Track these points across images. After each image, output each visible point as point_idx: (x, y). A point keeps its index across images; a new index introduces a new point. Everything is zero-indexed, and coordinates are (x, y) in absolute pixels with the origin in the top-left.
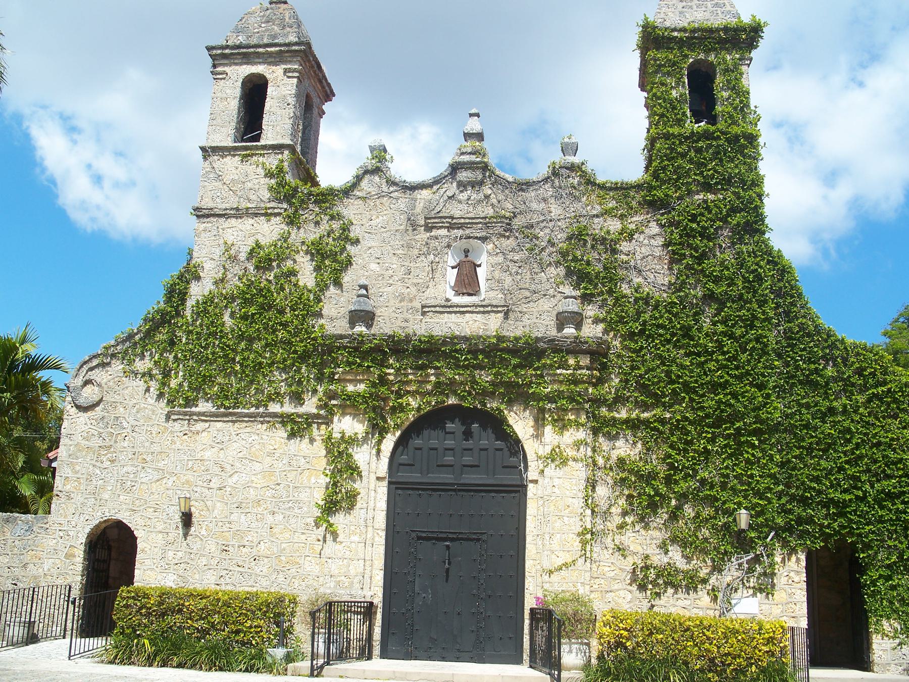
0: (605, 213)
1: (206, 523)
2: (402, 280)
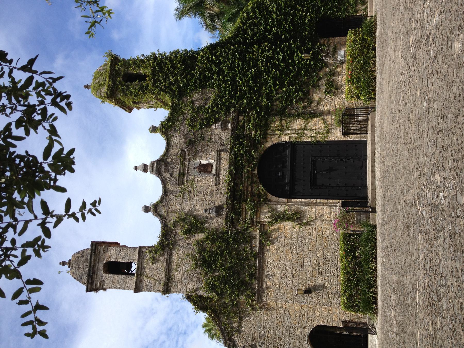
0: (175, 224)
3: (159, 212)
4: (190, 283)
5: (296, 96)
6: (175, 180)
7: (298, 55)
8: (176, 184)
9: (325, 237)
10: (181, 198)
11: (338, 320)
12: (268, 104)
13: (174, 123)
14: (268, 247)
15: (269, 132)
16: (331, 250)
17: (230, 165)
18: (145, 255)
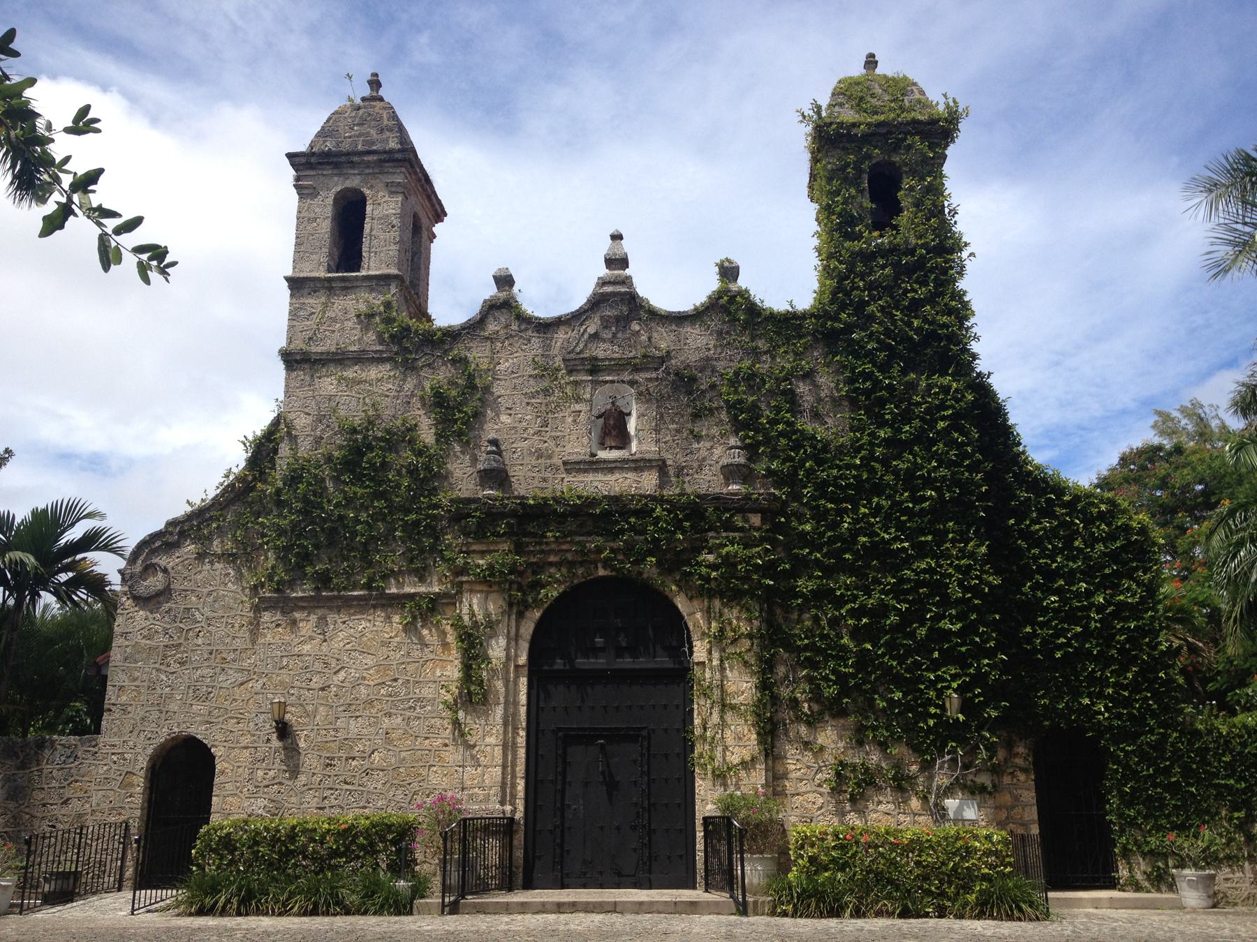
1: (305, 732)
2: (538, 433)
3: (493, 315)
4: (309, 420)
5: (826, 679)
6: (578, 350)
7: (954, 677)
8: (569, 353)
9: (424, 773)
10: (530, 371)
11: (227, 812)
12: (802, 595)
13: (745, 328)
14: (396, 618)
15: (717, 603)
16: (388, 791)
17: (615, 499)
18: (380, 292)
